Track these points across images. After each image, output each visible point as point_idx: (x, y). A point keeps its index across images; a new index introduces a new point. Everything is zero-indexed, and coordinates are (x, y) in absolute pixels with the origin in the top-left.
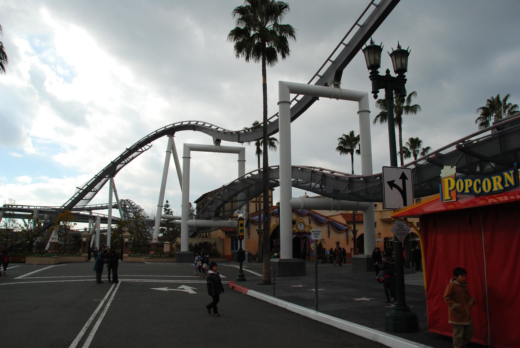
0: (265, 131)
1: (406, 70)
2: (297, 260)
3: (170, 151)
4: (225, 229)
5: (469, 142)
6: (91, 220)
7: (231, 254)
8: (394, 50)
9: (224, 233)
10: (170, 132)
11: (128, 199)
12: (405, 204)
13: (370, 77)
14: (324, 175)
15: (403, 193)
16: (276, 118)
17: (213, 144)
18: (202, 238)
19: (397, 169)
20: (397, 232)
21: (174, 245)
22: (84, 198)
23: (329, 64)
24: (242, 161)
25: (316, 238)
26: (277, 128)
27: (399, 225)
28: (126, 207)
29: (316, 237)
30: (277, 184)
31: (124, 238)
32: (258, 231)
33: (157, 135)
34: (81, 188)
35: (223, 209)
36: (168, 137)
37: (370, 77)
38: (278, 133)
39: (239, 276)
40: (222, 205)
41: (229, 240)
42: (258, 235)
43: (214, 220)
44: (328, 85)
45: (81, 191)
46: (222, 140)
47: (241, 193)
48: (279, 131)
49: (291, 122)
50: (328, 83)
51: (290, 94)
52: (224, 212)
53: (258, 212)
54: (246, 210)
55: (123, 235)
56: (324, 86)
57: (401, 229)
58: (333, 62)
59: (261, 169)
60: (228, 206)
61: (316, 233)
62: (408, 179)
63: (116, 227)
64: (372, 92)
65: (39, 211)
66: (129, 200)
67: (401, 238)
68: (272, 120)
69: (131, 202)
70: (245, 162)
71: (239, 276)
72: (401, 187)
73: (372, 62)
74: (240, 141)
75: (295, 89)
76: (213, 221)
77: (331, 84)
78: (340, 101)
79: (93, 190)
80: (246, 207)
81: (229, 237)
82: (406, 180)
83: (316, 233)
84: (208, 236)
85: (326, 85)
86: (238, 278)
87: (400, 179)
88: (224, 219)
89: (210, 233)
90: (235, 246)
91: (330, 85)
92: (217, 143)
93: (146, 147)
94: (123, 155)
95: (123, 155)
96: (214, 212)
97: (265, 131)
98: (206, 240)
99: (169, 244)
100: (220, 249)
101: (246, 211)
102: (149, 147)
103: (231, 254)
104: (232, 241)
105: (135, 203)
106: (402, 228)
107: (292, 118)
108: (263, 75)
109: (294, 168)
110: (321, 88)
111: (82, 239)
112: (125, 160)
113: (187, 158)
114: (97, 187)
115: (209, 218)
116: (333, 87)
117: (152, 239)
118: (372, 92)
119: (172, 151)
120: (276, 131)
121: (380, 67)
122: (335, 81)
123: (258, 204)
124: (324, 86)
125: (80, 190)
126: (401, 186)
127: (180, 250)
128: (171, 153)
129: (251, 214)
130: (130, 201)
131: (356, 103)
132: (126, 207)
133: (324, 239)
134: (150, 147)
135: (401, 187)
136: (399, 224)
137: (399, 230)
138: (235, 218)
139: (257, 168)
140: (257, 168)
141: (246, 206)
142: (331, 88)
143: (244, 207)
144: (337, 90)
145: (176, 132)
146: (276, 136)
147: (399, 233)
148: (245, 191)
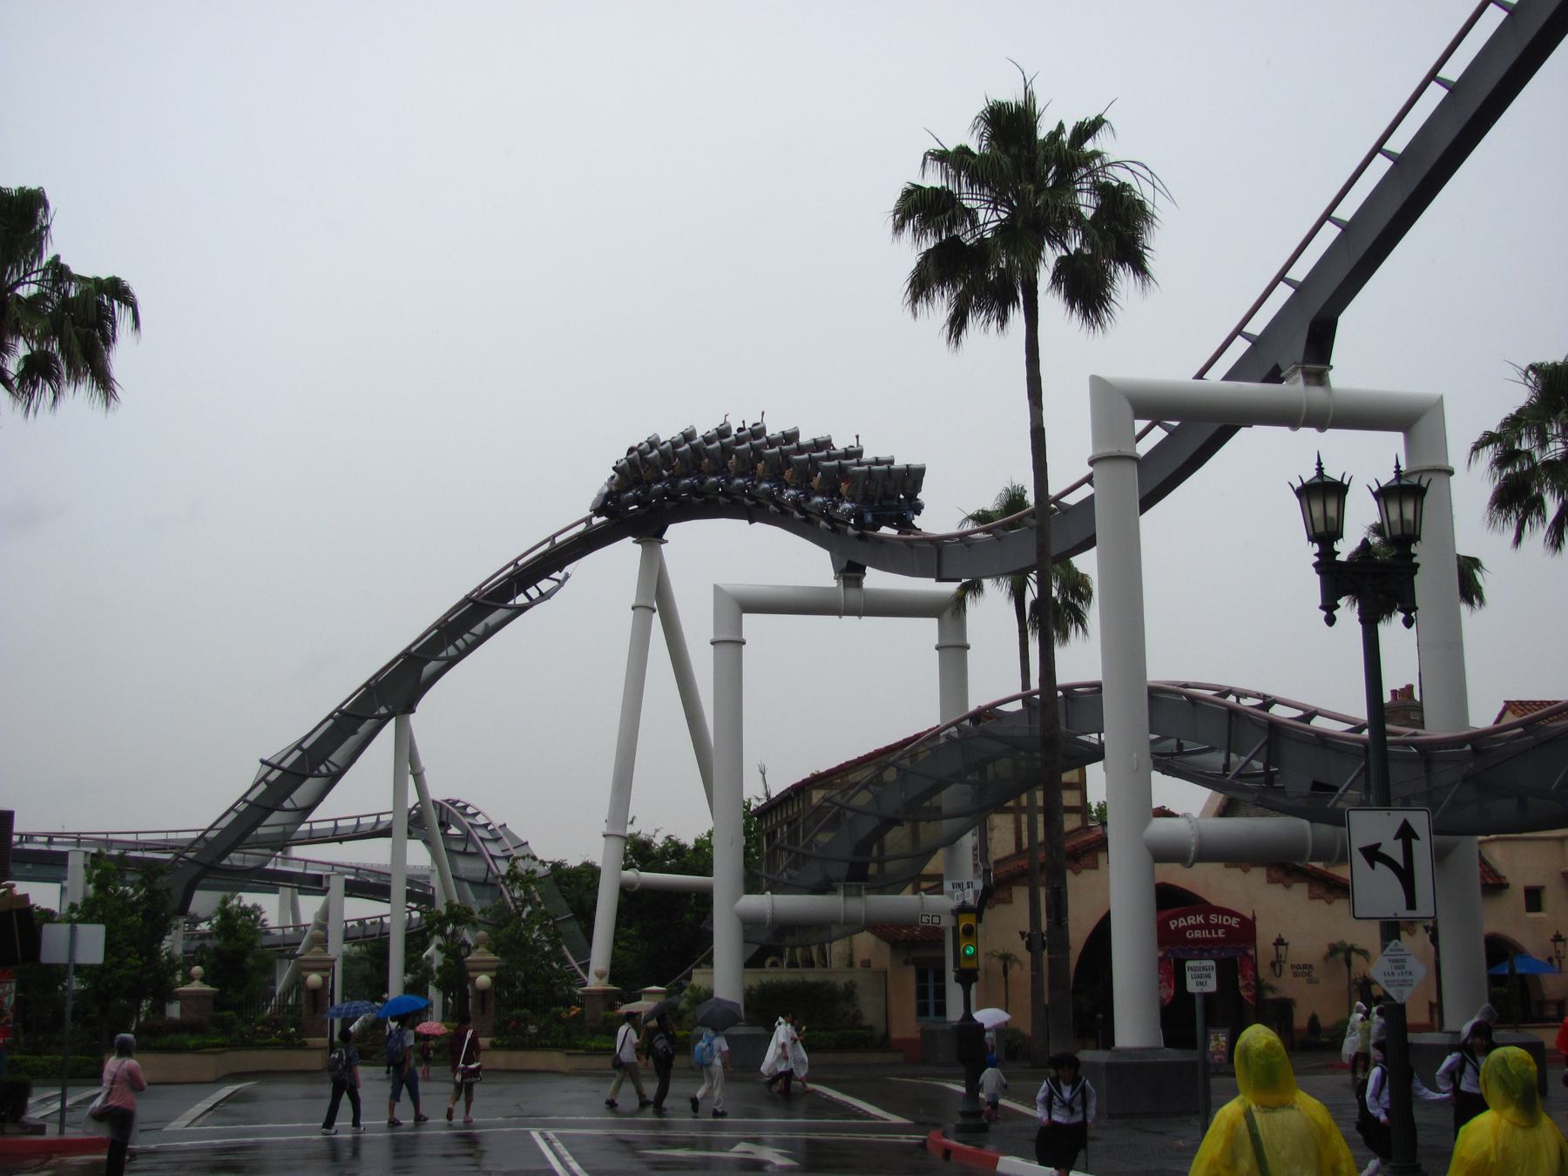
0: (1042, 533)
1: (1415, 538)
2: (1176, 1055)
3: (648, 604)
4: (884, 928)
6: (289, 889)
7: (918, 1035)
8: (1382, 485)
9: (886, 947)
11: (454, 797)
12: (1411, 904)
13: (1315, 565)
14: (1276, 729)
15: (1406, 875)
16: (1086, 491)
17: (834, 584)
18: (773, 970)
19: (1389, 814)
20: (1387, 978)
22: (287, 804)
23: (1283, 293)
24: (954, 649)
25: (1200, 987)
26: (1092, 533)
27: (1394, 961)
28: (450, 832)
29: (1201, 984)
30: (1097, 754)
31: (474, 970)
32: (1027, 939)
34: (275, 761)
35: (881, 849)
36: (639, 547)
37: (1315, 565)
38: (1094, 550)
39: (964, 1114)
40: (878, 835)
41: (909, 977)
42: (1029, 954)
43: (845, 895)
44: (1282, 375)
45: (276, 774)
46: (867, 568)
47: (954, 787)
48: (1095, 545)
49: (1141, 514)
50: (1282, 368)
51: (1136, 421)
52: (881, 863)
53: (1026, 851)
54: (975, 849)
55: (469, 961)
56: (1264, 381)
57: (1400, 971)
59: (1036, 693)
60: (897, 838)
61: (1199, 973)
62: (1418, 839)
63: (416, 915)
64: (1322, 608)
65: (89, 857)
66: (459, 805)
67: (1400, 995)
68: (1072, 499)
69: (470, 810)
70: (968, 651)
71: (964, 1114)
72: (1400, 860)
73: (1320, 528)
74: (944, 577)
75: (1150, 406)
76: (841, 898)
77: (1294, 371)
79: (323, 769)
80: (976, 839)
81: (906, 963)
82: (1413, 841)
83: (1199, 973)
84: (815, 959)
85: (1275, 376)
86: (960, 1121)
87: (1396, 838)
88: (881, 890)
89: (827, 946)
90: (931, 1001)
91: (1289, 375)
92: (850, 578)
93: (545, 585)
94: (450, 620)
95: (450, 620)
96: (846, 861)
97: (1042, 533)
98: (812, 976)
100: (869, 1009)
101: (976, 855)
102: (556, 583)
103: (918, 1035)
104: (921, 977)
105: (487, 818)
106: (1404, 967)
107: (1143, 498)
108: (1029, 398)
109: (1157, 695)
110: (1253, 390)
111: (306, 978)
112: (457, 642)
113: (730, 645)
114: (337, 757)
116: (1301, 383)
118: (1322, 608)
120: (1089, 543)
121: (1342, 537)
122: (1305, 361)
123: (1024, 818)
124: (1266, 380)
125: (270, 768)
126: (1399, 859)
128: (654, 611)
129: (997, 863)
130: (466, 806)
131: (1397, 438)
132: (450, 832)
133: (1311, 967)
134: (561, 583)
135: (1400, 860)
136: (1393, 957)
137: (1393, 973)
138: (927, 881)
139: (1018, 690)
140: (1018, 690)
141: (974, 835)
142: (1294, 389)
143: (969, 840)
144: (1316, 393)
145: (670, 526)
146: (1086, 563)
147: (1394, 981)
148: (969, 778)
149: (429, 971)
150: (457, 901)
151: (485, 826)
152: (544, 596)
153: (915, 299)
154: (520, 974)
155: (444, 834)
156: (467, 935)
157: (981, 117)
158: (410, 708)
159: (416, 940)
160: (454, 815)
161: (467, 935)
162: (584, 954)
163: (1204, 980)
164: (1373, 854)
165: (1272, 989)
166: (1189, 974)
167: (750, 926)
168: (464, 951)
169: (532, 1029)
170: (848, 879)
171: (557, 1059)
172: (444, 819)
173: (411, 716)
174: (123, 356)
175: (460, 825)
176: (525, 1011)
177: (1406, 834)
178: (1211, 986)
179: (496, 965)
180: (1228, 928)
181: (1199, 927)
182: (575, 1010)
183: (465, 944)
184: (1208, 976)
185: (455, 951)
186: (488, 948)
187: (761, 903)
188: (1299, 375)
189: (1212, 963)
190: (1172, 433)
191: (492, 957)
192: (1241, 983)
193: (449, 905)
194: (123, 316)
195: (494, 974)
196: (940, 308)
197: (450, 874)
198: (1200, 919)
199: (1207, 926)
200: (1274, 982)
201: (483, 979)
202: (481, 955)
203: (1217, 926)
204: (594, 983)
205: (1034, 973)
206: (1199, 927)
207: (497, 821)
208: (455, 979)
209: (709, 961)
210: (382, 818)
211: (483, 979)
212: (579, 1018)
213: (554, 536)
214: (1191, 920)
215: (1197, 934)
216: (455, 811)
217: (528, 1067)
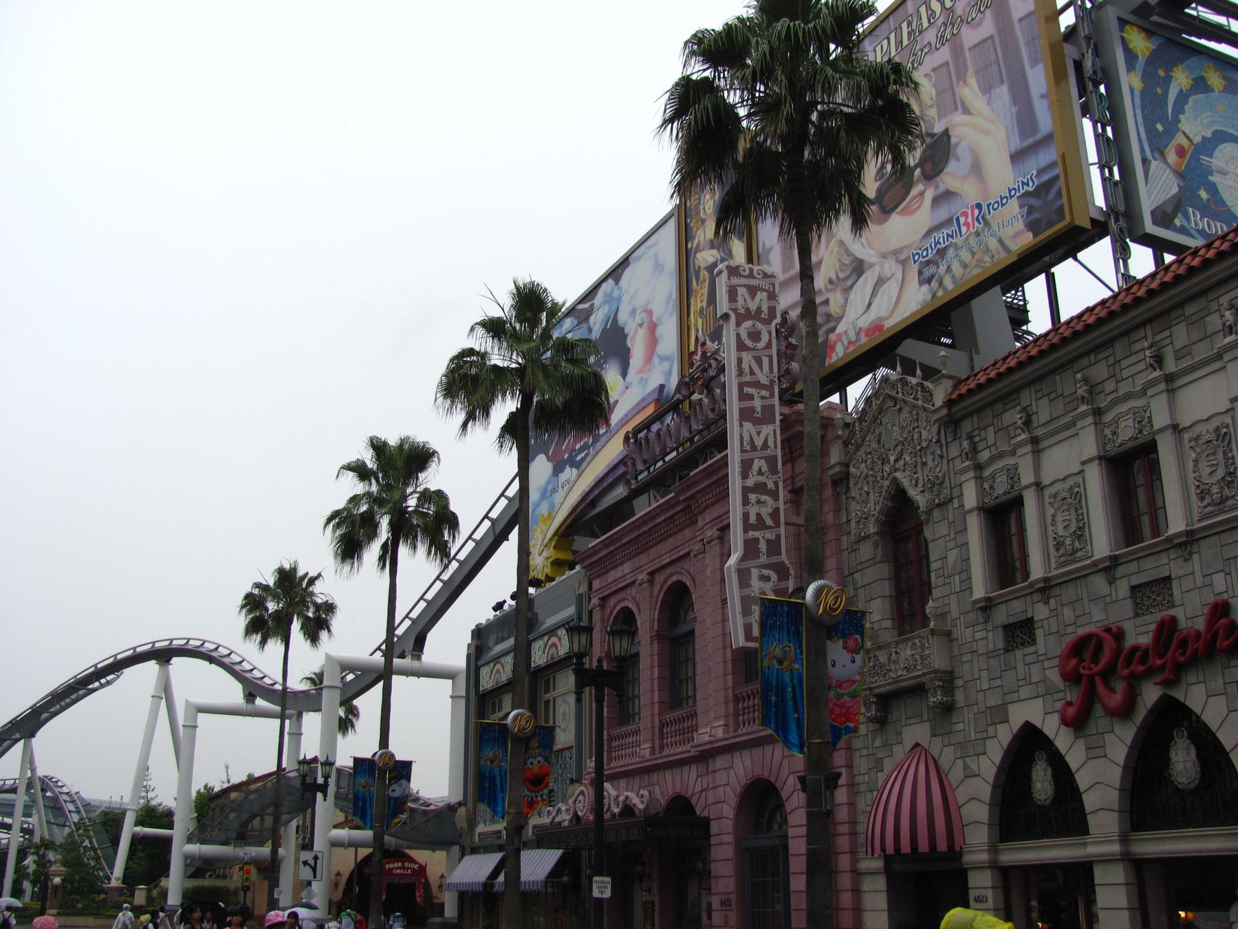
5: (1146, 520)
10: (163, 655)
21: (155, 893)
33: (137, 658)
43: (234, 846)
58: (477, 543)
69: (60, 784)
78: (422, 679)
81: (264, 879)
93: (110, 678)
98: (220, 883)
99: (145, 891)
115: (225, 843)
117: (109, 879)
119: (163, 696)
122: (413, 650)
126: (313, 865)
127: (166, 901)
130: (57, 782)
144: (416, 664)
150: (47, 837)
151: (67, 793)
152: (109, 683)
153: (246, 635)
154: (78, 877)
155: (44, 796)
156: (51, 856)
157: (276, 570)
158: (33, 736)
159: (22, 853)
160: (50, 786)
161: (51, 856)
162: (112, 866)
163: (603, 890)
164: (305, 863)
165: (436, 898)
166: (595, 885)
167: (189, 859)
169: (80, 906)
170: (237, 839)
172: (45, 787)
173: (33, 739)
175: (53, 791)
178: (607, 894)
179: (63, 873)
180: (413, 870)
181: (400, 868)
182: (103, 896)
183: (50, 861)
184: (606, 887)
185: (43, 863)
186: (61, 863)
187: (194, 848)
188: (410, 656)
189: (608, 879)
190: (357, 677)
191: (63, 869)
192: (417, 895)
193: (42, 839)
195: (63, 877)
196: (258, 638)
197: (44, 819)
198: (400, 864)
199: (403, 868)
200: (439, 895)
201: (57, 880)
203: (408, 868)
204: (114, 883)
206: (400, 868)
207: (74, 790)
208: (41, 878)
209: (168, 876)
210: (7, 782)
211: (57, 880)
212: (105, 899)
213: (116, 655)
214: (396, 865)
215: (398, 871)
216: (51, 784)
217: (75, 924)
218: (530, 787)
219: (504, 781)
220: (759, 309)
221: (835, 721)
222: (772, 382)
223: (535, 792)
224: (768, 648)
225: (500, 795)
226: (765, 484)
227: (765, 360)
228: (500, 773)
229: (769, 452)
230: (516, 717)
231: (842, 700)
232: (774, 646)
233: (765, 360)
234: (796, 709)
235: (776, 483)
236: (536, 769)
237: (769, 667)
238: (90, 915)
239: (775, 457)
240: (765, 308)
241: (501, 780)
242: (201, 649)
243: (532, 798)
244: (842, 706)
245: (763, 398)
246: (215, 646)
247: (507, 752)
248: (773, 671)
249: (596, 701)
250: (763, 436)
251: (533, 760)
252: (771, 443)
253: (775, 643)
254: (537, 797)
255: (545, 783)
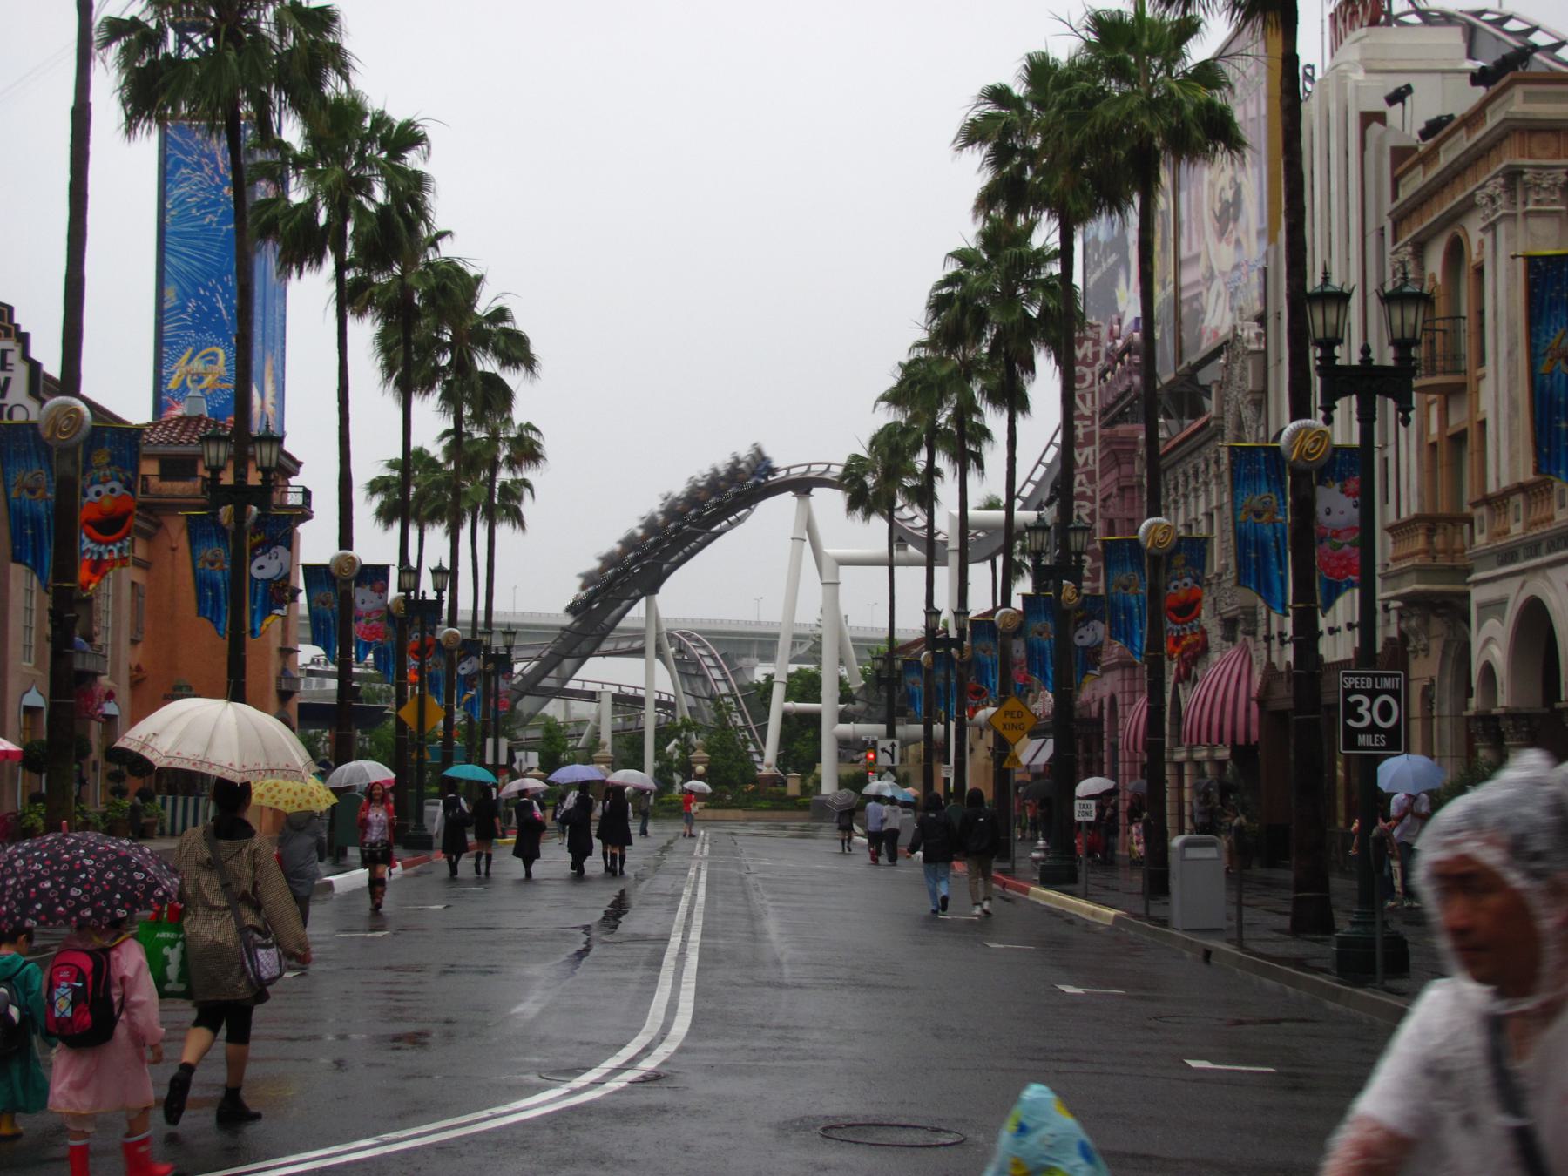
15: (892, 756)
149: (670, 761)
152: (739, 520)
156: (695, 740)
164: (883, 750)
168: (690, 750)
169: (729, 797)
171: (740, 813)
174: (527, 507)
176: (725, 787)
177: (893, 745)
185: (686, 748)
193: (683, 719)
194: (526, 492)
202: (699, 754)
205: (463, 784)
218: (1175, 617)
219: (1281, 547)
220: (1085, 356)
221: (1331, 575)
222: (1093, 413)
223: (1182, 623)
224: (1547, 341)
225: (1275, 574)
226: (1084, 492)
227: (1089, 397)
228: (1275, 534)
229: (1089, 468)
230: (1150, 527)
231: (1340, 552)
232: (1558, 337)
233: (1089, 397)
234: (1141, 627)
235: (1094, 491)
236: (1182, 594)
237: (1551, 374)
238: (740, 807)
239: (1094, 471)
240: (1090, 355)
241: (1277, 547)
242: (811, 475)
243: (1178, 632)
244: (1340, 558)
245: (1084, 426)
246: (825, 466)
247: (1284, 497)
248: (1560, 377)
249: (1359, 420)
250: (1084, 457)
251: (1176, 583)
252: (1090, 462)
253: (1561, 331)
254: (1184, 629)
255: (1195, 612)
